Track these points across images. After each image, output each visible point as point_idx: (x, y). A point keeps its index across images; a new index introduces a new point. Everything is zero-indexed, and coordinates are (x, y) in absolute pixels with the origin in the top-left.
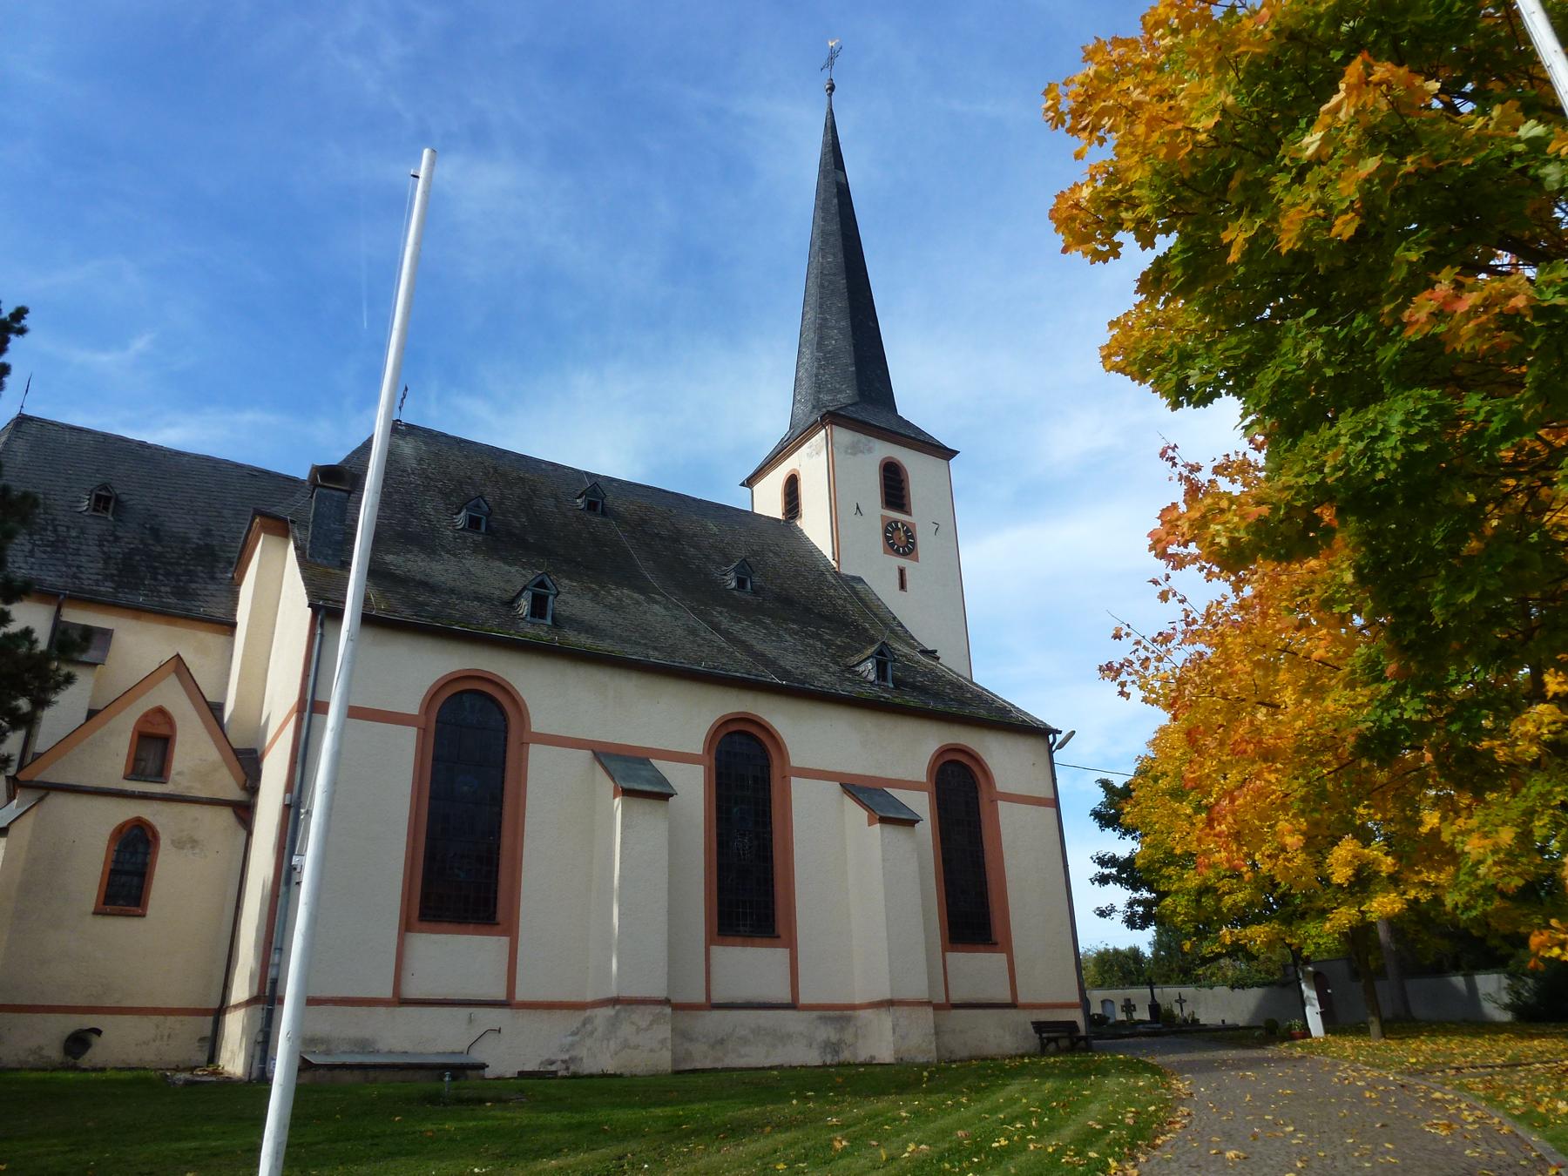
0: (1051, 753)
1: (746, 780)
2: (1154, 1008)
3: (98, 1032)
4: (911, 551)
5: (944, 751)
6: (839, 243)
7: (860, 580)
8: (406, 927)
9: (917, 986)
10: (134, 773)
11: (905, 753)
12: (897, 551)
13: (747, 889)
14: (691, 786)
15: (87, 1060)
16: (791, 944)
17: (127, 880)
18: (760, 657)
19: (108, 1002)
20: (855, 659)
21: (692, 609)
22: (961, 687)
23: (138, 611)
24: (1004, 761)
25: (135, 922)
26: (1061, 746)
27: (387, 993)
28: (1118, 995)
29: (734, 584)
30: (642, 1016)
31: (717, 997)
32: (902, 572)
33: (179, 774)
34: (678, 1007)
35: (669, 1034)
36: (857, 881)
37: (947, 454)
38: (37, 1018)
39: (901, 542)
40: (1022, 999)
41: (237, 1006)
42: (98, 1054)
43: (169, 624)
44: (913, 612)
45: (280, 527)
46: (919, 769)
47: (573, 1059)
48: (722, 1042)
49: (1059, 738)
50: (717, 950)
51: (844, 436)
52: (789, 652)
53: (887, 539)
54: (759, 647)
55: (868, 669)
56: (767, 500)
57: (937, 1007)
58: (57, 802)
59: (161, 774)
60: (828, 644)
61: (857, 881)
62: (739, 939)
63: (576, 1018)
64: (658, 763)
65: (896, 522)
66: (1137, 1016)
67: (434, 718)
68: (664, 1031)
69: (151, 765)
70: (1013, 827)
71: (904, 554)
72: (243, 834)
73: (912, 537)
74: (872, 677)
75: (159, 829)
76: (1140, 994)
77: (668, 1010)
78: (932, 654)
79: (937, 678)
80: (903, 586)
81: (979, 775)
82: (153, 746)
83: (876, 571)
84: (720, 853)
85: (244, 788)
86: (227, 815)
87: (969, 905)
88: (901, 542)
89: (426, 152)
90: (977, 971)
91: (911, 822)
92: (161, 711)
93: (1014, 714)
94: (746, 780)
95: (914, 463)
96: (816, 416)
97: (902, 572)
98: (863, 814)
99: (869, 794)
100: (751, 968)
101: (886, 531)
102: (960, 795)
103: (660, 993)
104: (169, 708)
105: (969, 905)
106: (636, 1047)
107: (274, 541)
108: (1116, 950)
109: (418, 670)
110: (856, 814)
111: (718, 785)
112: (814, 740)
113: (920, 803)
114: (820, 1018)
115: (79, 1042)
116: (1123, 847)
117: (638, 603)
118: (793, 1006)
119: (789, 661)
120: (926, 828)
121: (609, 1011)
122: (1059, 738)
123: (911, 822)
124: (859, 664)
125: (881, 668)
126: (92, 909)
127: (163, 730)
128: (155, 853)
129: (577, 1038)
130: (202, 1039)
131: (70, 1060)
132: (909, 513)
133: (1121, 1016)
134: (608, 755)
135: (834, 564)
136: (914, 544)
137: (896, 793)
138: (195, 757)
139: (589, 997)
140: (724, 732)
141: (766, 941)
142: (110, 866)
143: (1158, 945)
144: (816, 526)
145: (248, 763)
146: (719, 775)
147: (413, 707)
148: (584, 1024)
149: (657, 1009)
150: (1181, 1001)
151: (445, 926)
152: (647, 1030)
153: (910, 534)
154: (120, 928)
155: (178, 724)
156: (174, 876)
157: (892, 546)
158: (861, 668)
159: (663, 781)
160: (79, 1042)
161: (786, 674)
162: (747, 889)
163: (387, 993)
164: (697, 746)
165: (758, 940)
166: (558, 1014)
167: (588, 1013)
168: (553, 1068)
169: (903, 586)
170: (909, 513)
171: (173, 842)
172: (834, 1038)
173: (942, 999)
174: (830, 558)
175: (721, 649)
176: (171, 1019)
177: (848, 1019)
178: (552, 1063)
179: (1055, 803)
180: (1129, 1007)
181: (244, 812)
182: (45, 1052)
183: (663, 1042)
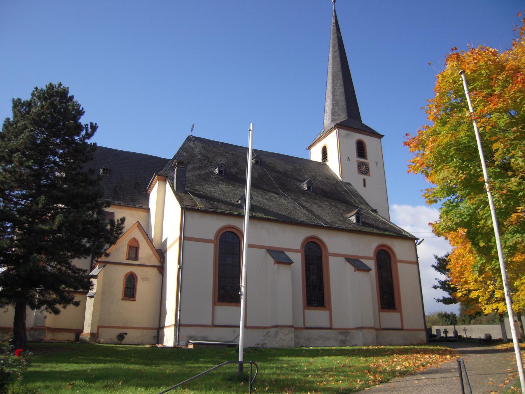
0: (416, 246)
1: (314, 258)
2: (456, 332)
3: (126, 334)
4: (367, 172)
5: (379, 246)
6: (339, 60)
7: (349, 184)
8: (214, 304)
9: (370, 322)
10: (129, 259)
11: (366, 247)
12: (362, 173)
13: (316, 292)
14: (297, 259)
15: (125, 340)
16: (330, 310)
17: (130, 290)
18: (317, 216)
19: (128, 326)
20: (348, 215)
21: (293, 199)
22: (385, 223)
23: (121, 206)
24: (399, 248)
25: (133, 302)
26: (419, 244)
27: (210, 323)
28: (442, 328)
29: (306, 188)
30: (285, 331)
31: (307, 325)
32: (364, 180)
33: (141, 258)
34: (296, 329)
35: (293, 336)
36: (351, 292)
37: (380, 136)
38: (110, 330)
39: (363, 169)
40: (405, 327)
41: (169, 326)
42: (126, 340)
43: (130, 210)
44: (369, 195)
45: (165, 178)
46: (371, 253)
47: (264, 344)
48: (309, 339)
49: (419, 241)
50: (307, 311)
51: (344, 132)
52: (325, 211)
53: (359, 169)
54: (317, 213)
55: (353, 219)
56: (316, 155)
57: (377, 330)
58: (108, 266)
59: (136, 258)
60: (339, 210)
61: (351, 292)
62: (313, 308)
63: (265, 331)
64: (286, 253)
65: (362, 162)
66: (449, 335)
67: (218, 240)
68: (292, 335)
69: (133, 256)
70: (403, 272)
71: (365, 174)
72: (161, 276)
73: (368, 167)
74: (355, 221)
75: (137, 275)
76: (450, 328)
77: (293, 329)
78: (375, 211)
79: (377, 220)
80: (365, 185)
81: (392, 255)
82: (134, 250)
83: (356, 181)
84: (307, 281)
85: (160, 261)
86: (155, 270)
87: (388, 296)
88: (363, 169)
89: (251, 124)
90: (390, 319)
91: (368, 270)
92: (135, 239)
93: (404, 233)
94: (314, 258)
95: (367, 140)
96: (333, 125)
97: (364, 180)
98: (352, 268)
99: (356, 263)
100: (317, 317)
101: (358, 166)
102: (385, 260)
103: (291, 324)
104: (136, 238)
105: (388, 296)
106: (284, 340)
107: (162, 183)
108: (80, 258)
109: (211, 226)
110: (350, 268)
111: (306, 259)
112: (336, 244)
113: (371, 264)
114: (339, 332)
115: (121, 337)
116: (443, 277)
117: (276, 198)
118: (331, 328)
119: (326, 218)
120: (373, 272)
121: (275, 329)
122: (419, 241)
123: (368, 270)
124: (350, 217)
125: (358, 219)
126: (121, 298)
127: (135, 245)
128: (137, 281)
129: (265, 337)
130: (154, 337)
131: (119, 342)
132: (366, 159)
133: (443, 335)
134: (270, 250)
135: (340, 179)
136: (368, 170)
137: (364, 261)
138: (145, 253)
139: (269, 326)
140: (307, 242)
141: (321, 308)
142: (125, 286)
143: (462, 310)
144: (334, 165)
145: (161, 253)
146: (306, 256)
147: (212, 237)
148: (267, 333)
149: (289, 329)
150: (465, 330)
151: (225, 303)
152: (287, 335)
153: (367, 167)
154: (129, 304)
155: (140, 242)
156: (143, 288)
157: (360, 171)
158: (351, 219)
159: (289, 259)
160: (121, 337)
161: (326, 222)
162: (316, 292)
163: (210, 323)
164: (298, 247)
165: (319, 308)
166: (260, 330)
167: (268, 330)
168: (259, 346)
169: (365, 185)
170: (366, 159)
171: (141, 279)
172: (344, 339)
173: (379, 327)
174: (339, 176)
175: (304, 214)
176: (145, 331)
177: (348, 333)
178: (258, 344)
179: (417, 263)
180: (446, 332)
181: (162, 269)
182: (113, 339)
183: (292, 339)
